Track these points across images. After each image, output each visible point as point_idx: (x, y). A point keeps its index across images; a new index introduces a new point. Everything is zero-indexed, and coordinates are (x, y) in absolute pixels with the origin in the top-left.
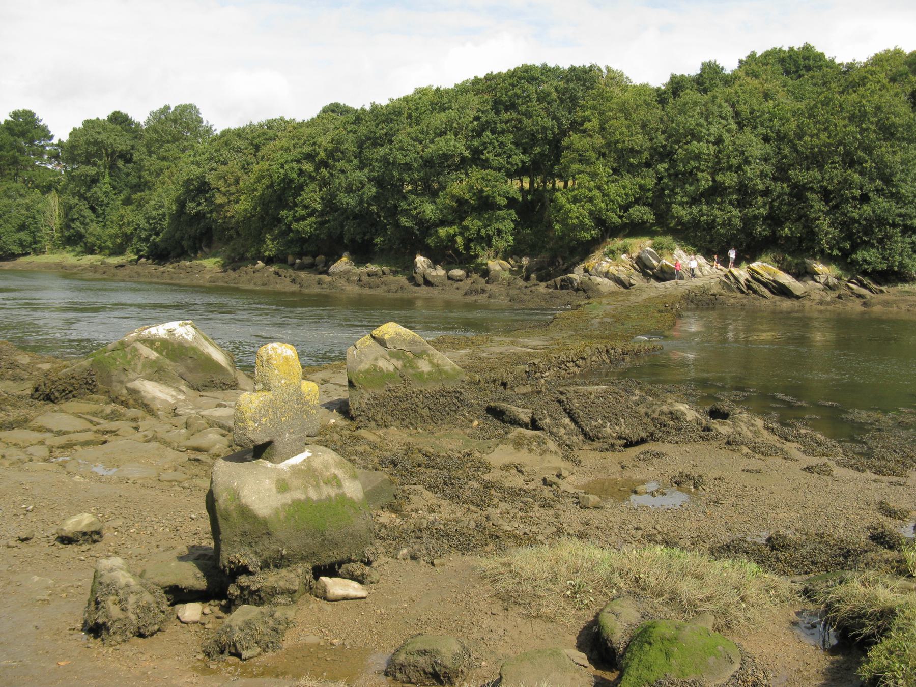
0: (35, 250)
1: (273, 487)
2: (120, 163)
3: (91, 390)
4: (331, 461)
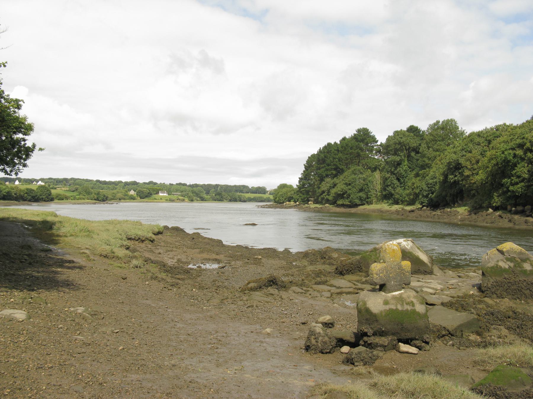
0: (367, 203)
1: (382, 302)
2: (413, 154)
3: (359, 271)
4: (412, 295)
